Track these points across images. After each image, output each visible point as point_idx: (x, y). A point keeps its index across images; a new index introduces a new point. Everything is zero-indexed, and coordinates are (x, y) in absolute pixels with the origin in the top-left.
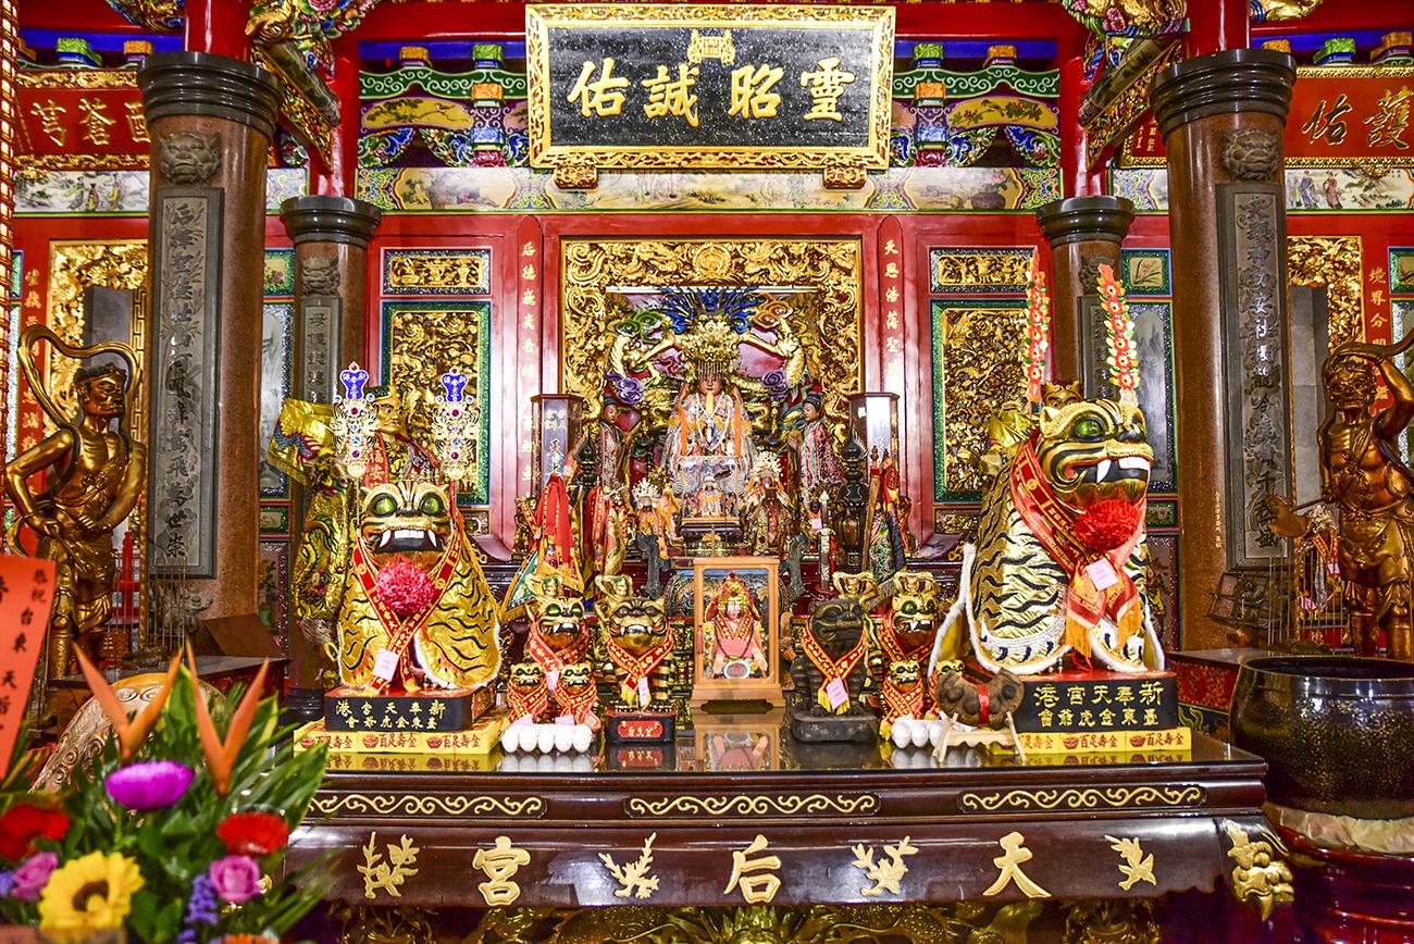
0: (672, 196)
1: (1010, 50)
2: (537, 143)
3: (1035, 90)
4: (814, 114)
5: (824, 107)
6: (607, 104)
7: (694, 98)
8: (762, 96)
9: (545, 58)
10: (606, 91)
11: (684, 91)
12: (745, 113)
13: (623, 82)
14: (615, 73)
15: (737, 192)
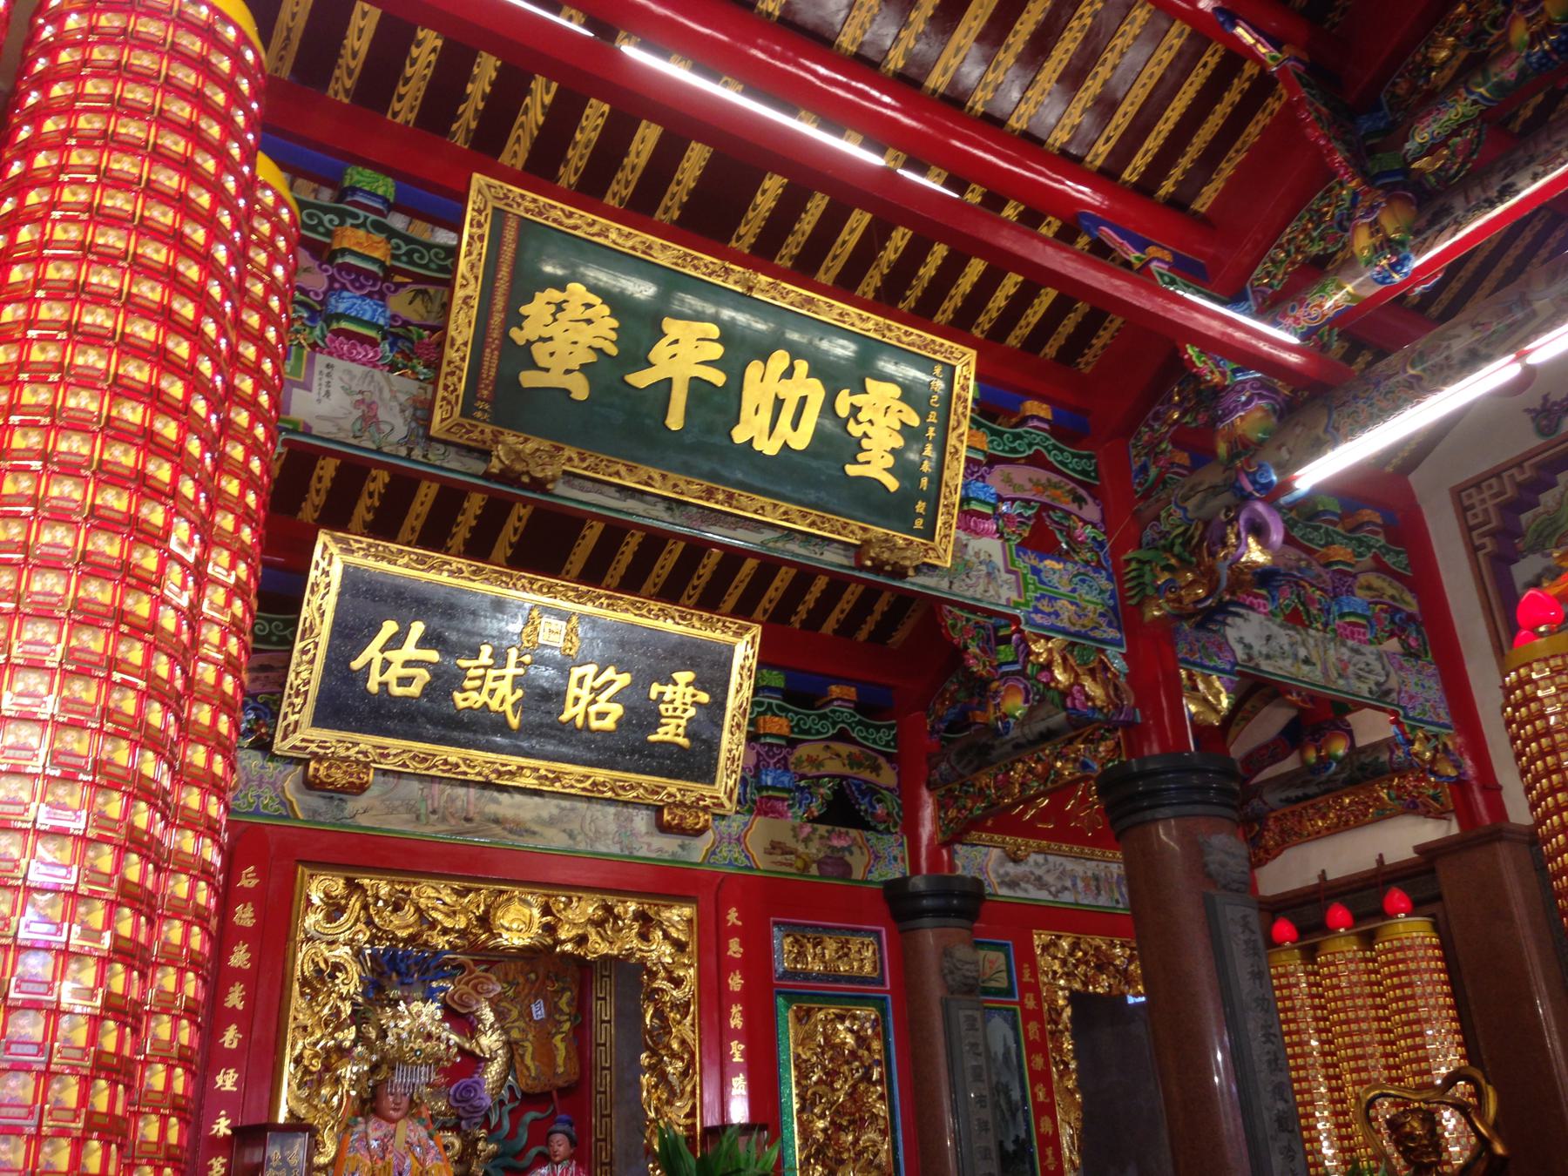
0: (468, 820)
1: (851, 692)
2: (292, 718)
3: (874, 741)
4: (659, 736)
5: (671, 729)
6: (405, 681)
7: (519, 693)
8: (602, 705)
9: (330, 603)
10: (407, 664)
11: (508, 681)
12: (579, 722)
13: (433, 656)
14: (423, 643)
15: (552, 822)
